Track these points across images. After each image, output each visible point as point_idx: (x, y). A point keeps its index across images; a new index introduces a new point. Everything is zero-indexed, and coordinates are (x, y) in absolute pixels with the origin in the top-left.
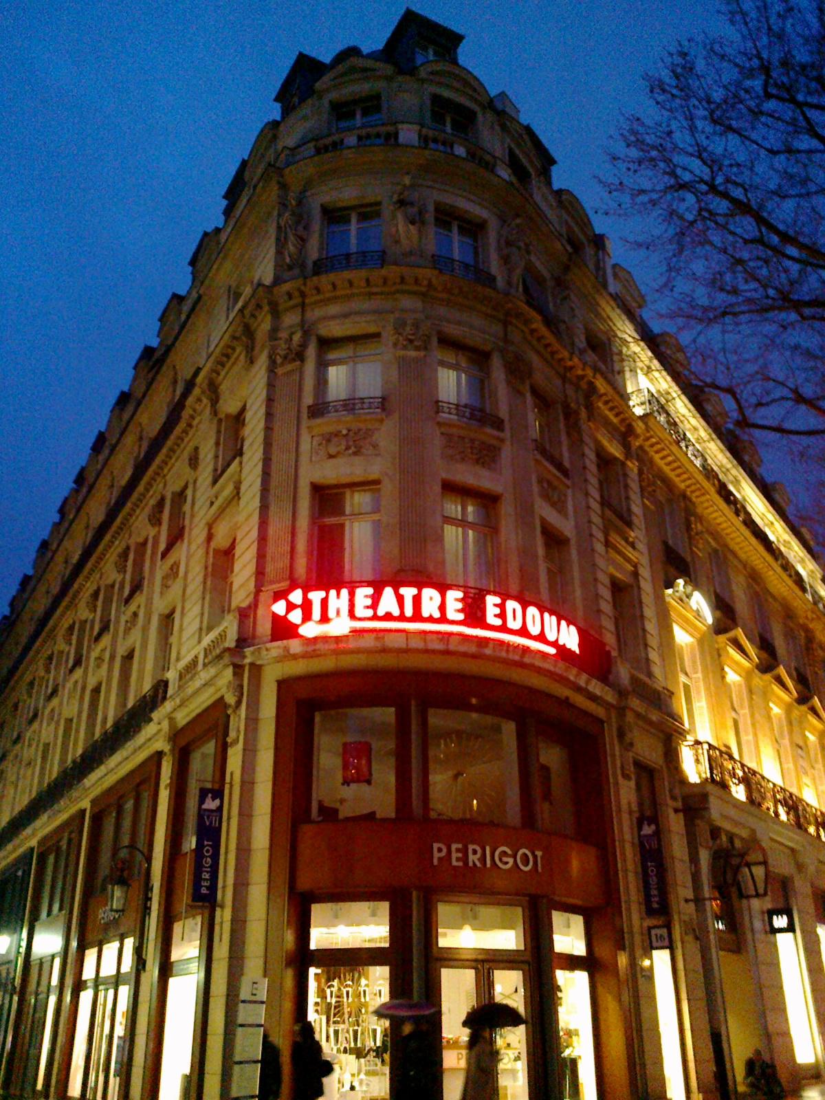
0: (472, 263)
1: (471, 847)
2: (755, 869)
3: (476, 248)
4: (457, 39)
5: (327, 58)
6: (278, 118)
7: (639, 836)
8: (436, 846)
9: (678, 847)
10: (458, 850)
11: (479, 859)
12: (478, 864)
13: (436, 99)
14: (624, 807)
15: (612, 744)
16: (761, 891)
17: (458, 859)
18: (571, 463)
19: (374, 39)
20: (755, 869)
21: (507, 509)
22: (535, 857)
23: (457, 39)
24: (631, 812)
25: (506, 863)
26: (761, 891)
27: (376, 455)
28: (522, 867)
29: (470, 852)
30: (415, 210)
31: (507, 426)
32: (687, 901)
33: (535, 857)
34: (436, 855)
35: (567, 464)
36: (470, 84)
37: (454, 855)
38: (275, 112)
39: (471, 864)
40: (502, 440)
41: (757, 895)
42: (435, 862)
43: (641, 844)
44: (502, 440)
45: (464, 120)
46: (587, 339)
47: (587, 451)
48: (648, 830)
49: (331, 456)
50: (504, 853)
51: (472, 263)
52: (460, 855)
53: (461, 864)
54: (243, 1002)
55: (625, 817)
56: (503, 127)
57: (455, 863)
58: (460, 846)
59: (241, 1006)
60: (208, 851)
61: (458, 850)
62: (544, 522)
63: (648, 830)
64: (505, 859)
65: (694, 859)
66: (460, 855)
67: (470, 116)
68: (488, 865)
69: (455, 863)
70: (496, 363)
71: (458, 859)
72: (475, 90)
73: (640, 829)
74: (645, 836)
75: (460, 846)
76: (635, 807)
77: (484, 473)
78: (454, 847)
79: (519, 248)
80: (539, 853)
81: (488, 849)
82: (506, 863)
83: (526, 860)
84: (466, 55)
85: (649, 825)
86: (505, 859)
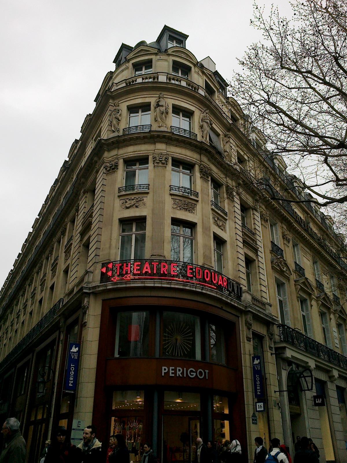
0: (187, 128)
1: (178, 368)
2: (307, 379)
3: (190, 123)
4: (186, 37)
5: (133, 45)
6: (113, 70)
7: (253, 364)
8: (163, 368)
9: (271, 369)
10: (172, 370)
11: (164, 373)
12: (181, 376)
13: (174, 62)
14: (247, 352)
15: (242, 327)
16: (310, 388)
17: (172, 373)
18: (229, 210)
19: (151, 38)
20: (307, 379)
21: (199, 229)
22: (205, 373)
23: (186, 37)
24: (250, 355)
25: (193, 375)
26: (310, 388)
27: (145, 208)
28: (200, 377)
29: (178, 370)
30: (164, 108)
31: (200, 195)
32: (275, 392)
33: (205, 373)
34: (163, 371)
35: (227, 210)
36: (189, 56)
37: (171, 371)
38: (112, 67)
39: (178, 375)
40: (197, 201)
41: (308, 390)
42: (163, 375)
43: (254, 368)
44: (197, 201)
45: (186, 70)
46: (238, 158)
47: (236, 205)
48: (256, 362)
49: (127, 208)
50: (192, 371)
51: (187, 128)
52: (173, 371)
53: (173, 375)
54: (74, 429)
55: (247, 357)
56: (203, 73)
57: (171, 375)
58: (173, 368)
59: (73, 431)
60: (72, 369)
61: (172, 370)
62: (214, 233)
63: (256, 362)
64: (192, 373)
65: (279, 374)
66: (173, 371)
67: (190, 69)
68: (185, 376)
69: (171, 375)
70: (197, 168)
71: (172, 373)
72: (191, 58)
73: (253, 361)
74: (256, 364)
75: (173, 368)
76: (252, 352)
77: (190, 214)
78: (171, 368)
79: (207, 123)
80: (207, 371)
81: (185, 369)
82: (193, 375)
83: (201, 373)
84: (189, 45)
85: (257, 360)
86: (192, 373)
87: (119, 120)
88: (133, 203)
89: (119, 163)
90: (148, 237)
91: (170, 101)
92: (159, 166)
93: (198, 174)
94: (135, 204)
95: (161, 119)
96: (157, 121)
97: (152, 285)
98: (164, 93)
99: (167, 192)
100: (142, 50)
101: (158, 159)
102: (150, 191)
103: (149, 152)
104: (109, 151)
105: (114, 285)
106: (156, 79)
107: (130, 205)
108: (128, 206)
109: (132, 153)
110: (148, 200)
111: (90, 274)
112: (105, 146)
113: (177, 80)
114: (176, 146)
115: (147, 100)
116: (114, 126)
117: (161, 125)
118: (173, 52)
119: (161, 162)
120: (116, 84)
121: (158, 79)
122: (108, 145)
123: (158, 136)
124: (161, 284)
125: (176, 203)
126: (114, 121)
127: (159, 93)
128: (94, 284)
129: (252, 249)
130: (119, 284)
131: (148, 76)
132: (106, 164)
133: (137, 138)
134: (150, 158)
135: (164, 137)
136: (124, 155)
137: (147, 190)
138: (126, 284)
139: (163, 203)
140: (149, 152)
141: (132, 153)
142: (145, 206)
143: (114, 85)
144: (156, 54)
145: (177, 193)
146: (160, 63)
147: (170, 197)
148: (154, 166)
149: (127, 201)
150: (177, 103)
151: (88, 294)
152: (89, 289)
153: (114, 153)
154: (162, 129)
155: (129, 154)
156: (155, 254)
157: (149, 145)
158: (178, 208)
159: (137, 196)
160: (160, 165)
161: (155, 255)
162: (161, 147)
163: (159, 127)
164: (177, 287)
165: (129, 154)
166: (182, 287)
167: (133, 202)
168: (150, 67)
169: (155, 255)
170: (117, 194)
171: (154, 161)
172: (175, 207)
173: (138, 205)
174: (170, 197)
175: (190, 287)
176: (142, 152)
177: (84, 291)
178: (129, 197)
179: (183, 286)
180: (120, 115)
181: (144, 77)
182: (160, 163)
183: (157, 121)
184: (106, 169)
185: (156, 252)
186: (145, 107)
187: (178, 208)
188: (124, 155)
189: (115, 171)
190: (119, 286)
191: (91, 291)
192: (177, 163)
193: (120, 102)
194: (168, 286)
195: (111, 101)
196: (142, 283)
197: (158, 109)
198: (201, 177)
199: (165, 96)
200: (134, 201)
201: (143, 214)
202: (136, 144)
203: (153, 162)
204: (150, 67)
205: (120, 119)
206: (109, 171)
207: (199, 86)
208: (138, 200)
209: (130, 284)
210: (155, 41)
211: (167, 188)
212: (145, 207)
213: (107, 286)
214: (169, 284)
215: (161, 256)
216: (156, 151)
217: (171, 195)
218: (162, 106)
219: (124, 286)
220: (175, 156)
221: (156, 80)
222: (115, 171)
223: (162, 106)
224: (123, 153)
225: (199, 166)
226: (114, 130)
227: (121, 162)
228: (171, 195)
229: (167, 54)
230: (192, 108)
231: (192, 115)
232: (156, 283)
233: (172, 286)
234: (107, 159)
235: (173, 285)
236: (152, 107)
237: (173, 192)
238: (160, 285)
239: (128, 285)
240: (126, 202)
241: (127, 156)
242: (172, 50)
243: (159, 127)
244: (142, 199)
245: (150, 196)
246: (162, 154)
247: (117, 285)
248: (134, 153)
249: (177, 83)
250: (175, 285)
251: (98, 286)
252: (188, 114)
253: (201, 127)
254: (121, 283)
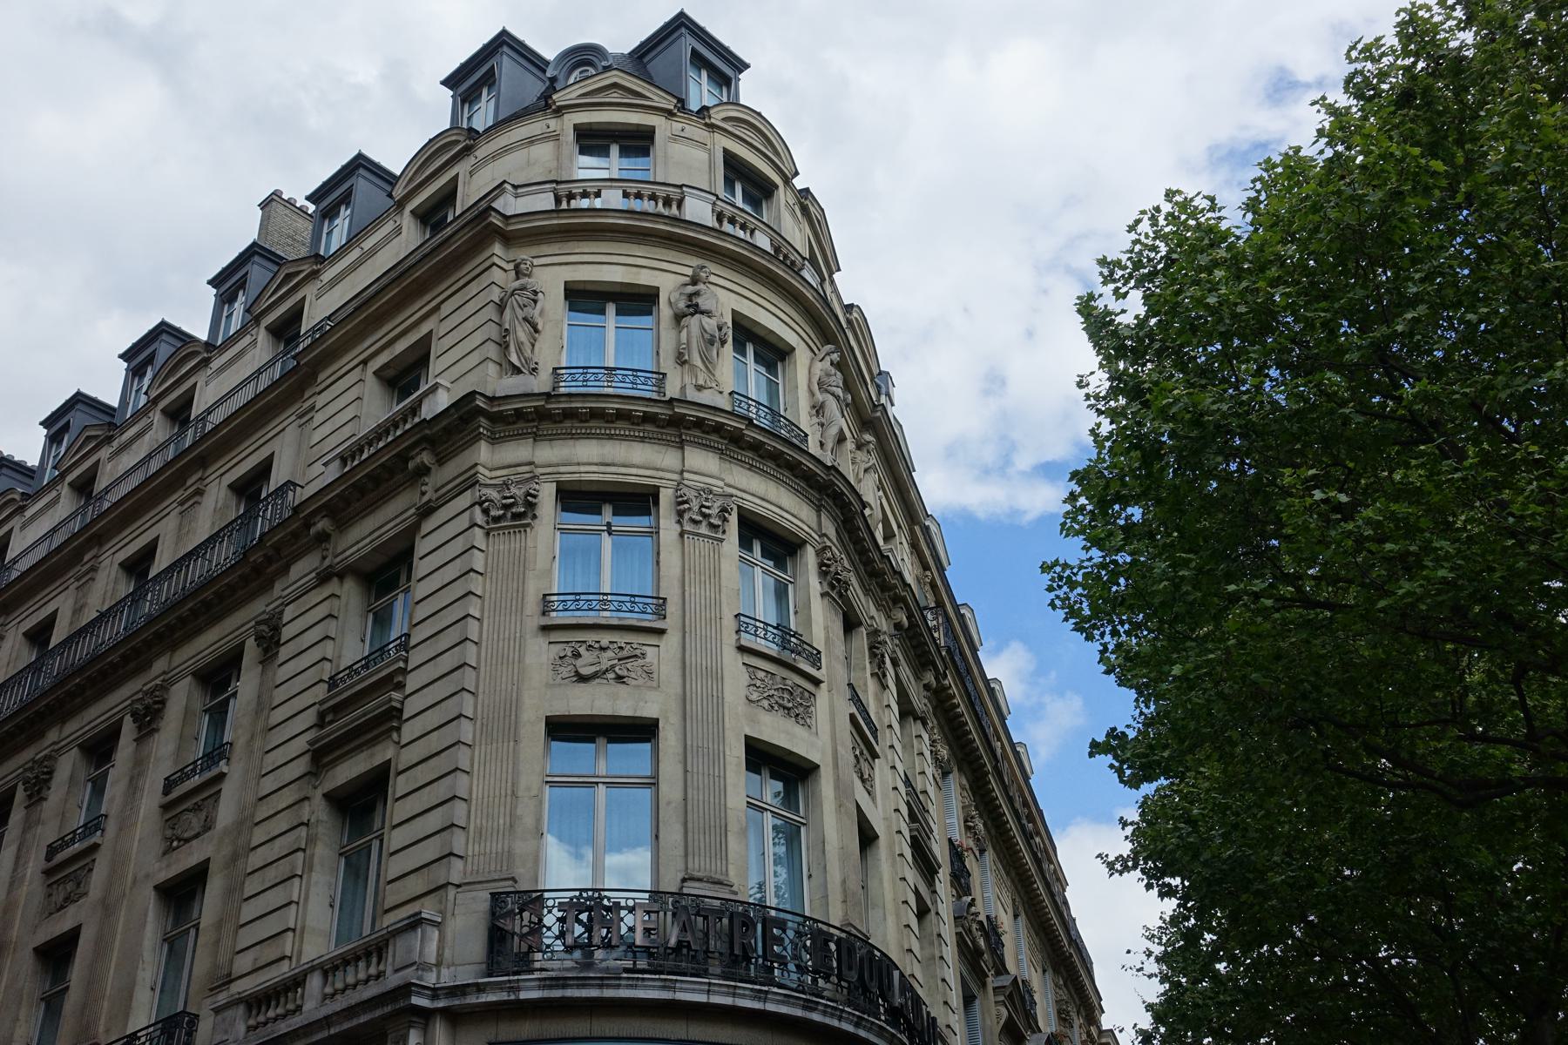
13: (731, 161)
23: (741, 66)
27: (651, 688)
49: (582, 679)
70: (810, 557)
87: (537, 331)
88: (605, 664)
89: (541, 494)
90: (669, 803)
91: (729, 297)
92: (698, 535)
93: (669, 528)
94: (613, 666)
95: (706, 360)
96: (685, 362)
97: (702, 998)
98: (712, 267)
99: (730, 639)
100: (615, 85)
101: (696, 508)
102: (671, 623)
103: (660, 474)
104: (494, 440)
105: (551, 987)
106: (674, 206)
107: (593, 669)
108: (585, 671)
109: (594, 468)
110: (663, 655)
111: (429, 929)
112: (483, 421)
113: (743, 227)
114: (751, 468)
115: (645, 278)
116: (520, 351)
117: (701, 382)
118: (725, 119)
119: (700, 516)
120: (515, 187)
121: (679, 207)
122: (495, 418)
123: (699, 424)
124: (734, 995)
125: (758, 683)
126: (519, 329)
127: (696, 262)
128: (447, 978)
129: (369, 736)
130: (571, 986)
131: (647, 190)
132: (484, 491)
133: (621, 415)
134: (666, 496)
135: (718, 429)
136: (562, 469)
137: (649, 621)
138: (601, 986)
139: (717, 676)
140: (660, 474)
141: (594, 468)
142: (651, 679)
143: (504, 191)
144: (669, 114)
145: (761, 645)
146: (678, 149)
147: (739, 656)
148: (682, 535)
149: (582, 650)
150: (747, 309)
151: (426, 1015)
152: (435, 993)
153: (518, 451)
154: (705, 398)
155: (583, 469)
156: (700, 874)
157: (656, 447)
158: (766, 703)
159: (621, 639)
160: (704, 529)
161: (699, 880)
162: (703, 463)
163: (699, 388)
164: (784, 1009)
165: (583, 469)
166: (799, 1013)
167: (606, 660)
168: (645, 152)
169: (699, 880)
170: (534, 620)
171: (680, 514)
172: (755, 696)
173: (625, 673)
174: (740, 658)
175: (824, 1013)
176: (634, 471)
177: (415, 1000)
178: (591, 637)
179: (805, 1008)
180: (542, 313)
181: (633, 188)
182: (704, 523)
183: (685, 362)
184: (486, 512)
185: (699, 866)
186: (638, 301)
187: (766, 703)
188: (562, 469)
189: (528, 525)
190: (569, 993)
191: (441, 1004)
192: (755, 530)
193: (536, 262)
194: (757, 1005)
195: (497, 248)
196: (664, 988)
197: (694, 322)
198: (823, 595)
199: (713, 279)
200: (610, 654)
201: (648, 711)
202: (611, 437)
203: (674, 518)
204: (645, 152)
205: (540, 327)
206: (497, 519)
207: (681, 187)
208: (625, 653)
209: (618, 986)
210: (626, 52)
211: (729, 623)
212: (649, 683)
213: (519, 989)
214: (759, 999)
215: (720, 883)
216: (686, 475)
217: (742, 649)
218: (708, 313)
219: (594, 993)
220: (747, 505)
221: (674, 211)
222: (528, 525)
223: (708, 313)
224: (555, 460)
225: (819, 553)
226: (517, 363)
227: (547, 495)
228: (742, 649)
229: (706, 125)
230: (790, 337)
231: (783, 360)
232: (715, 993)
233: (771, 1007)
234: (487, 473)
235: (773, 1001)
236: (665, 311)
237: (747, 640)
238: (728, 1001)
239: (609, 993)
240: (577, 655)
241: (575, 477)
242: (724, 115)
243: (699, 388)
244: (638, 652)
245: (671, 642)
246: (711, 492)
247: (564, 987)
248: (602, 469)
249: (741, 234)
250: (779, 1002)
251: (480, 988)
252: (773, 354)
253: (819, 409)
254: (583, 982)
